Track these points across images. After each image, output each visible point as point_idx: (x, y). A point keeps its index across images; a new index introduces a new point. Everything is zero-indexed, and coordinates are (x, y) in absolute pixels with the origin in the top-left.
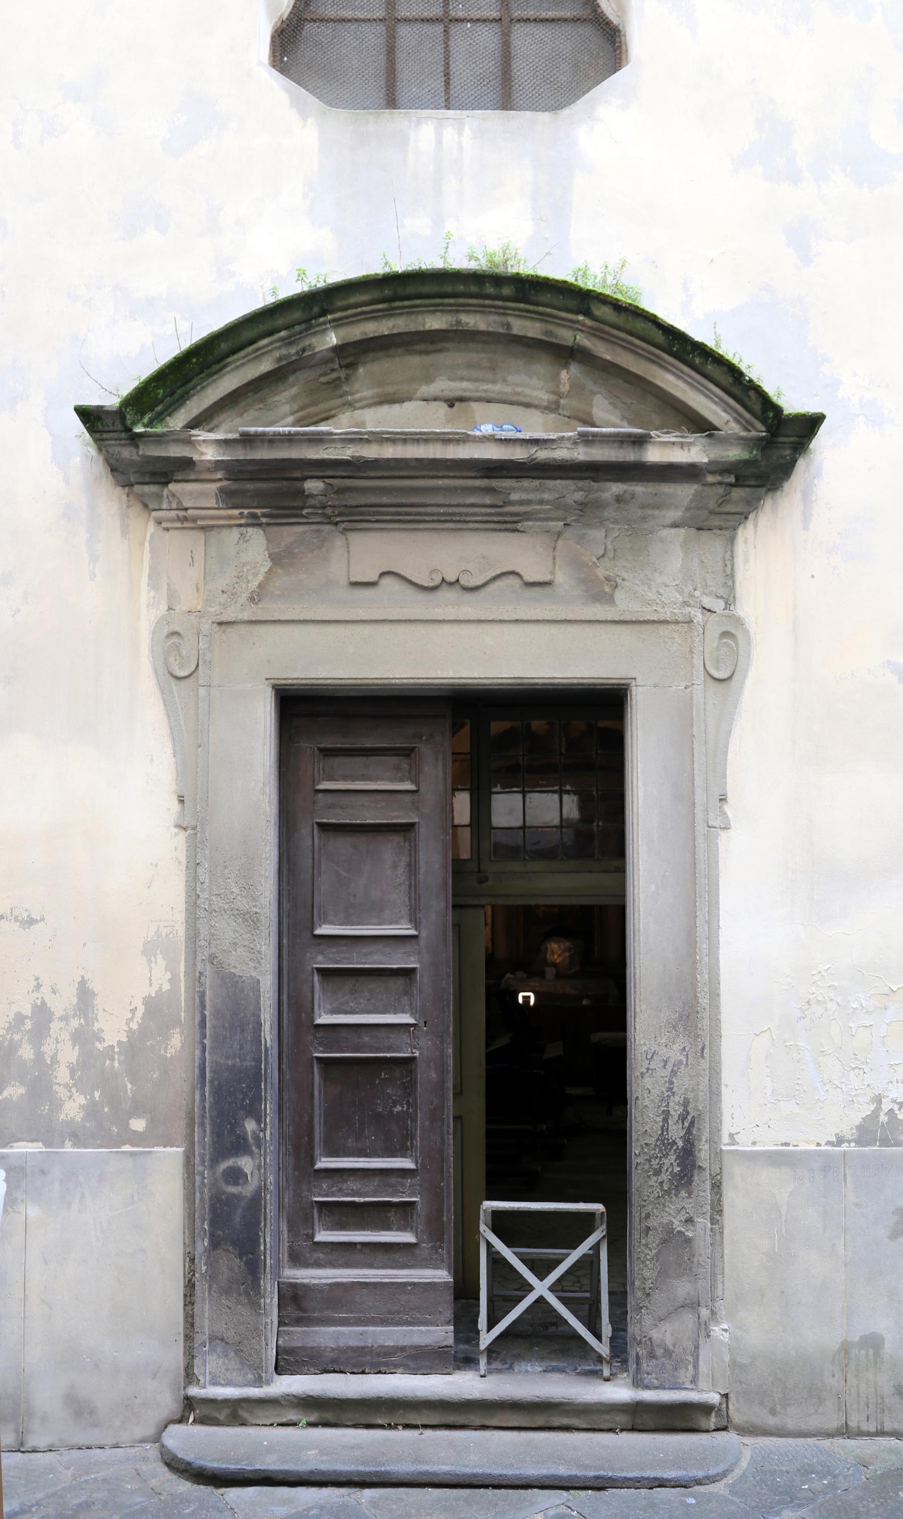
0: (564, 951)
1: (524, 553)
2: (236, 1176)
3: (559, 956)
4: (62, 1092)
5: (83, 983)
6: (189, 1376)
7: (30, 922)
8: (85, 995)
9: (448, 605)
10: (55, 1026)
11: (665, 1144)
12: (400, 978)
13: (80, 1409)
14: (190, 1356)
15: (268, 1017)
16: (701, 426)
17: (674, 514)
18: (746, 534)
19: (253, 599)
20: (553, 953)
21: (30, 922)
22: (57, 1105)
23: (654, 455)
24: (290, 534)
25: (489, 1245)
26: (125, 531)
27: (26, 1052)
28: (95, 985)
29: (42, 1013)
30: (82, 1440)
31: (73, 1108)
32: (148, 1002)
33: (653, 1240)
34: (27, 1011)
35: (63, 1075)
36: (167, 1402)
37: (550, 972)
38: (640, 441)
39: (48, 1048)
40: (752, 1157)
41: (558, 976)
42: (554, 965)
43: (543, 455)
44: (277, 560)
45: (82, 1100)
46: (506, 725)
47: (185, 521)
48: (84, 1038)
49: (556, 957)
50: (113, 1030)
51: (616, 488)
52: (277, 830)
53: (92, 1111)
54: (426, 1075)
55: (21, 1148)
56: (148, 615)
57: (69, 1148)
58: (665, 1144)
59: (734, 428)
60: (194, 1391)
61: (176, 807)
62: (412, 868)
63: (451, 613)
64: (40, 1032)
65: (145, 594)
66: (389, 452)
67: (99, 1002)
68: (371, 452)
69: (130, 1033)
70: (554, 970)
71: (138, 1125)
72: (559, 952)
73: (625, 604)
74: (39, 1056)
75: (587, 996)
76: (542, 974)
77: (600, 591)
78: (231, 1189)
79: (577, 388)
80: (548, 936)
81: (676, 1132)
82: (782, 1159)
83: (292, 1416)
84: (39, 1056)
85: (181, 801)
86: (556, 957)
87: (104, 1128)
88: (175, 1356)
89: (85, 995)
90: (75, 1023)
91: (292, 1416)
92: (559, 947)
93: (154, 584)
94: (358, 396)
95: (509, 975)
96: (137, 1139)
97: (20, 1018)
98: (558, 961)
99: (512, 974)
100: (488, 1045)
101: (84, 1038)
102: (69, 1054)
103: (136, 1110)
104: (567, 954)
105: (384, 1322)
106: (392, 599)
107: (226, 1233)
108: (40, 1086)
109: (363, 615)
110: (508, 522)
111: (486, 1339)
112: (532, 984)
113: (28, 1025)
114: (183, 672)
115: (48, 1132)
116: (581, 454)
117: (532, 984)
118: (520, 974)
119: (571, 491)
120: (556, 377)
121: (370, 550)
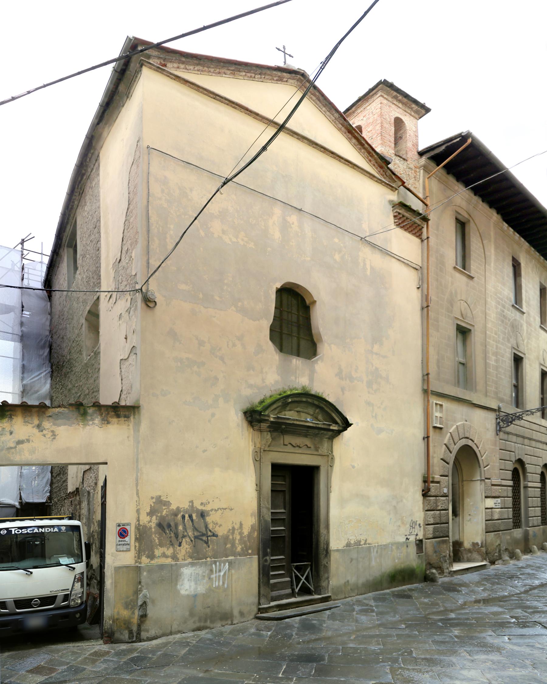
1: (307, 441)
2: (266, 560)
4: (237, 545)
5: (241, 522)
6: (259, 604)
7: (232, 509)
8: (241, 524)
9: (297, 450)
10: (236, 531)
11: (324, 548)
13: (242, 614)
14: (259, 600)
16: (336, 423)
17: (327, 436)
18: (334, 440)
19: (269, 446)
21: (232, 509)
22: (236, 548)
23: (331, 428)
24: (275, 434)
25: (295, 573)
26: (248, 430)
27: (231, 537)
28: (243, 523)
29: (234, 529)
30: (242, 620)
31: (239, 549)
32: (252, 526)
33: (322, 567)
34: (231, 528)
35: (237, 542)
36: (255, 609)
38: (330, 425)
39: (234, 536)
40: (334, 550)
43: (318, 426)
44: (273, 439)
45: (240, 547)
47: (261, 431)
48: (241, 533)
50: (246, 532)
51: (322, 432)
53: (242, 549)
54: (287, 539)
55: (230, 558)
56: (251, 448)
57: (238, 557)
58: (324, 548)
59: (341, 424)
60: (260, 607)
61: (255, 486)
62: (285, 499)
63: (298, 452)
64: (233, 533)
65: (251, 443)
66: (298, 423)
67: (244, 526)
68: (295, 422)
69: (249, 532)
71: (250, 551)
73: (320, 452)
74: (233, 538)
77: (317, 449)
78: (266, 563)
79: (318, 413)
81: (325, 547)
82: (338, 550)
83: (275, 609)
84: (233, 538)
85: (257, 485)
87: (244, 553)
88: (256, 600)
89: (241, 524)
90: (239, 531)
91: (275, 609)
93: (252, 442)
94: (44, 373)
96: (250, 554)
97: (230, 530)
101: (241, 533)
102: (238, 537)
103: (249, 549)
105: (281, 590)
106: (289, 448)
107: (265, 572)
108: (233, 545)
109: (286, 451)
110: (306, 436)
111: (297, 590)
113: (231, 531)
114: (258, 460)
115: (234, 554)
116: (323, 426)
119: (316, 431)
120: (315, 411)
121: (288, 439)
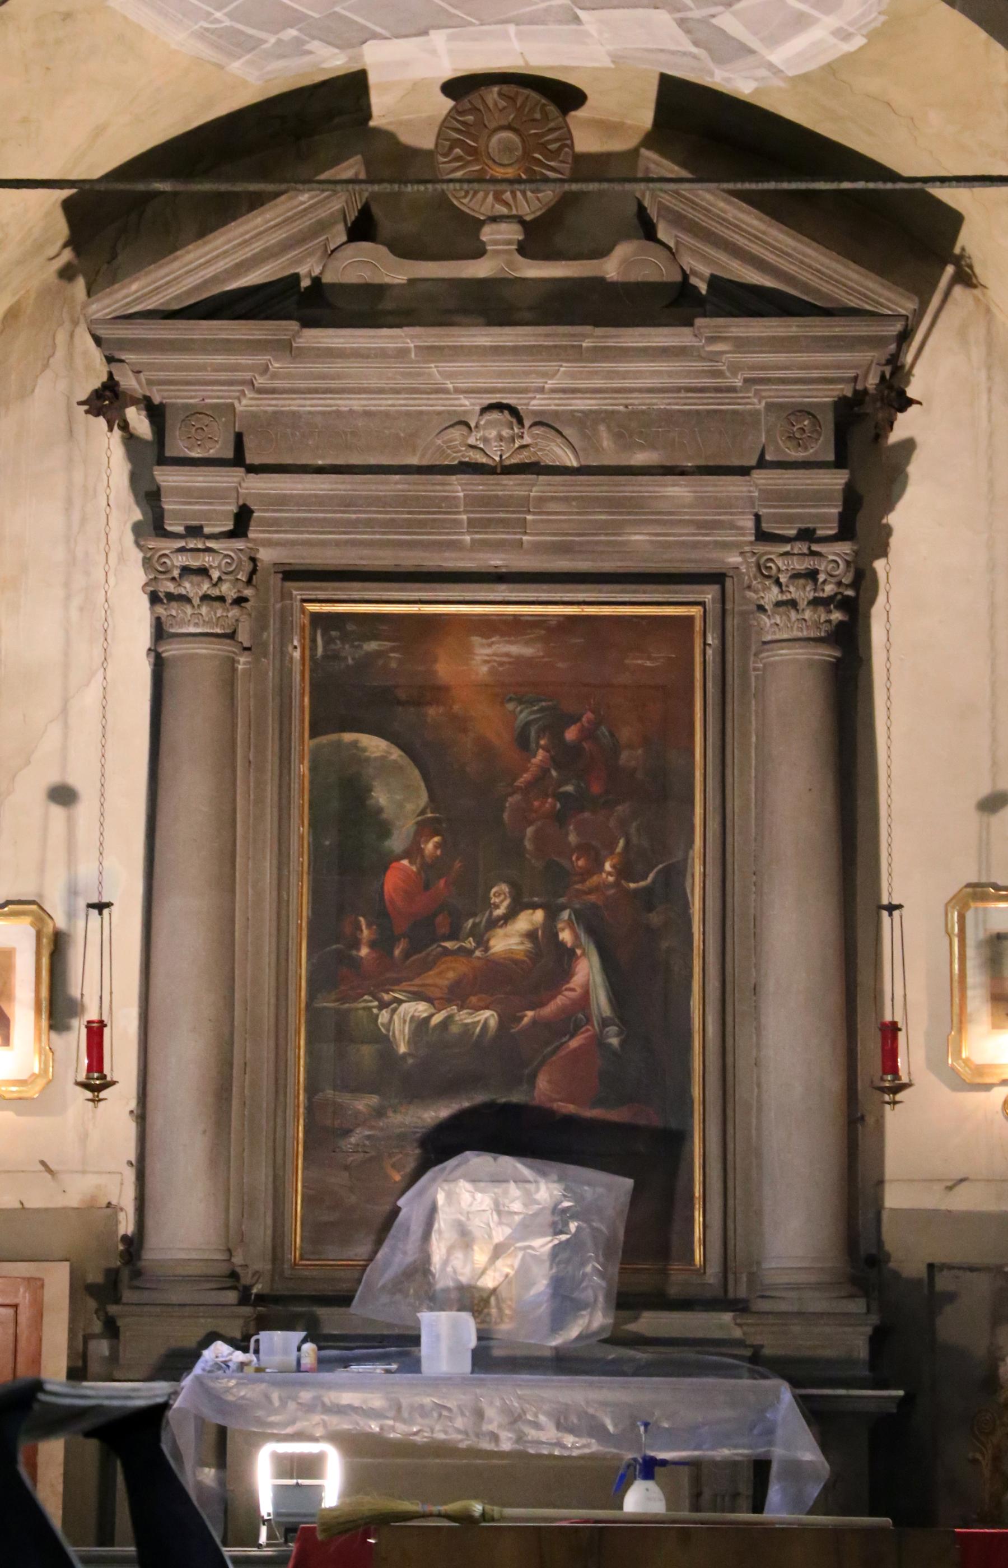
0: (527, 1228)
3: (498, 1251)
12: (609, 280)
15: (756, 277)
20: (465, 1238)
37: (445, 1338)
41: (486, 1359)
42: (473, 1300)
46: (354, 627)
49: (480, 1256)
52: (612, 571)
70: (468, 1325)
72: (501, 1234)
75: (649, 1468)
76: (400, 1347)
80: (440, 1147)
86: (480, 1256)
92: (499, 1209)
95: (220, 1350)
98: (489, 1282)
99: (241, 1344)
100: (173, 1435)
104: (543, 1244)
112: (347, 1398)
117: (347, 1398)
118: (280, 1345)
